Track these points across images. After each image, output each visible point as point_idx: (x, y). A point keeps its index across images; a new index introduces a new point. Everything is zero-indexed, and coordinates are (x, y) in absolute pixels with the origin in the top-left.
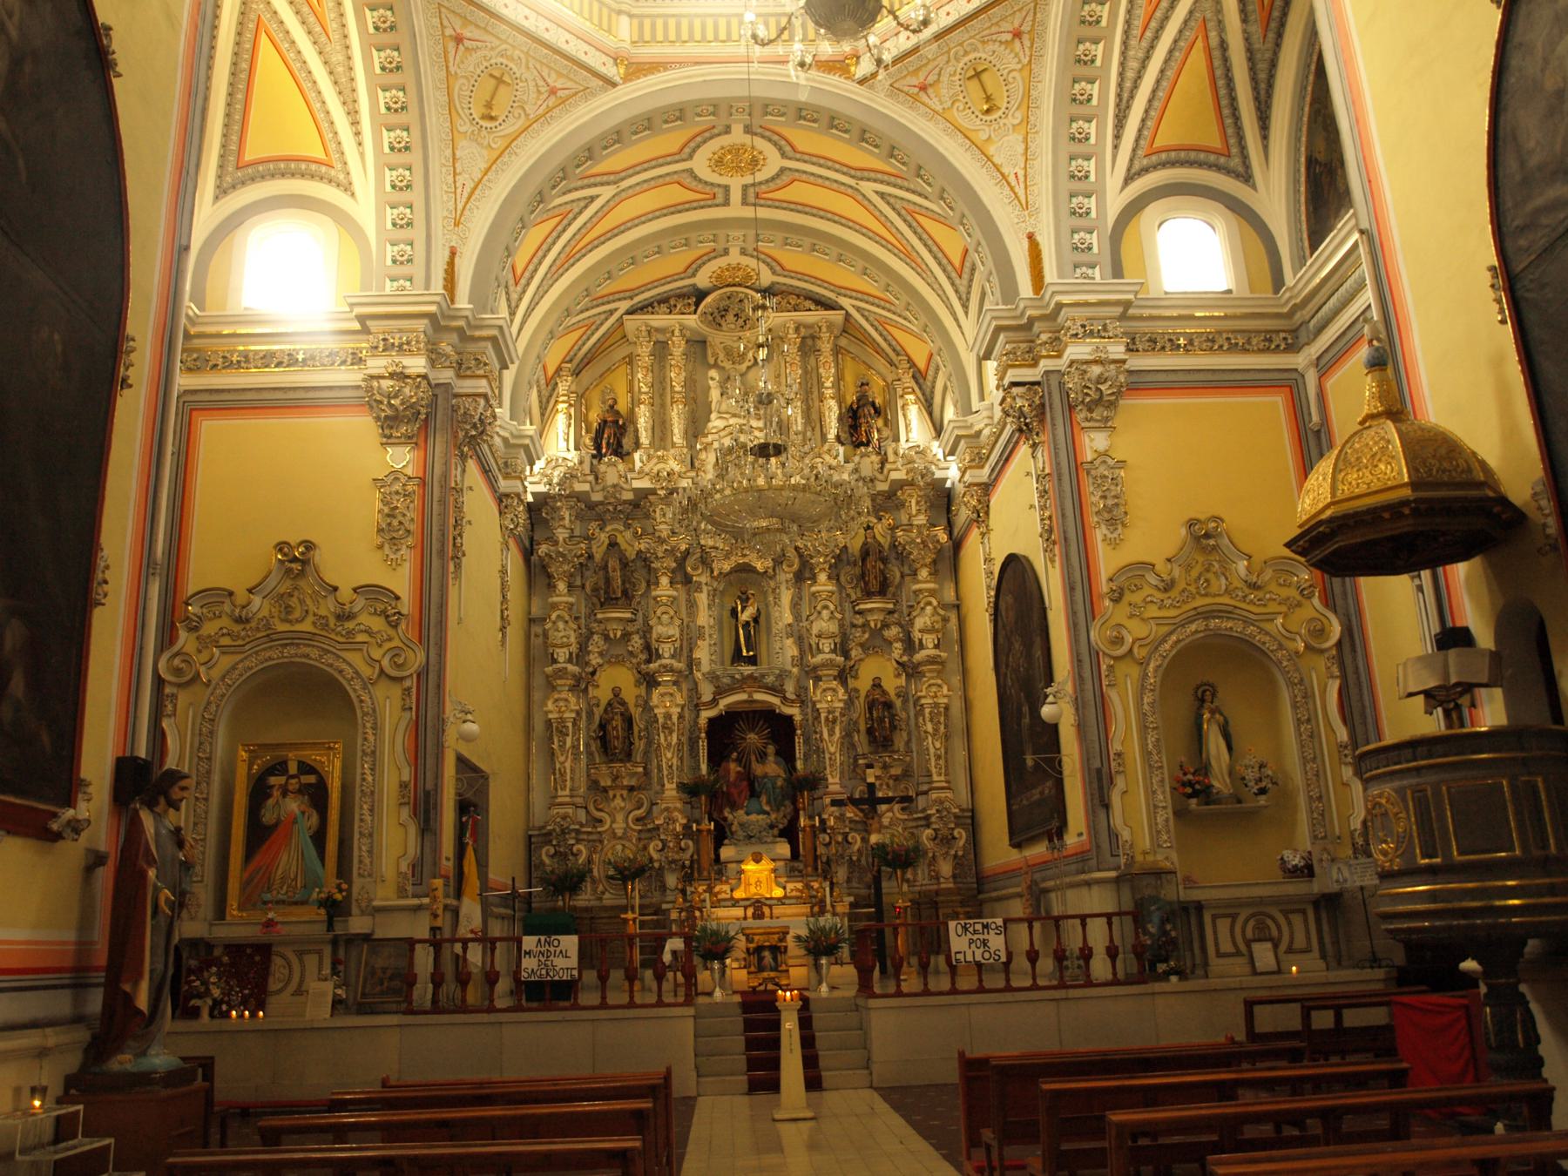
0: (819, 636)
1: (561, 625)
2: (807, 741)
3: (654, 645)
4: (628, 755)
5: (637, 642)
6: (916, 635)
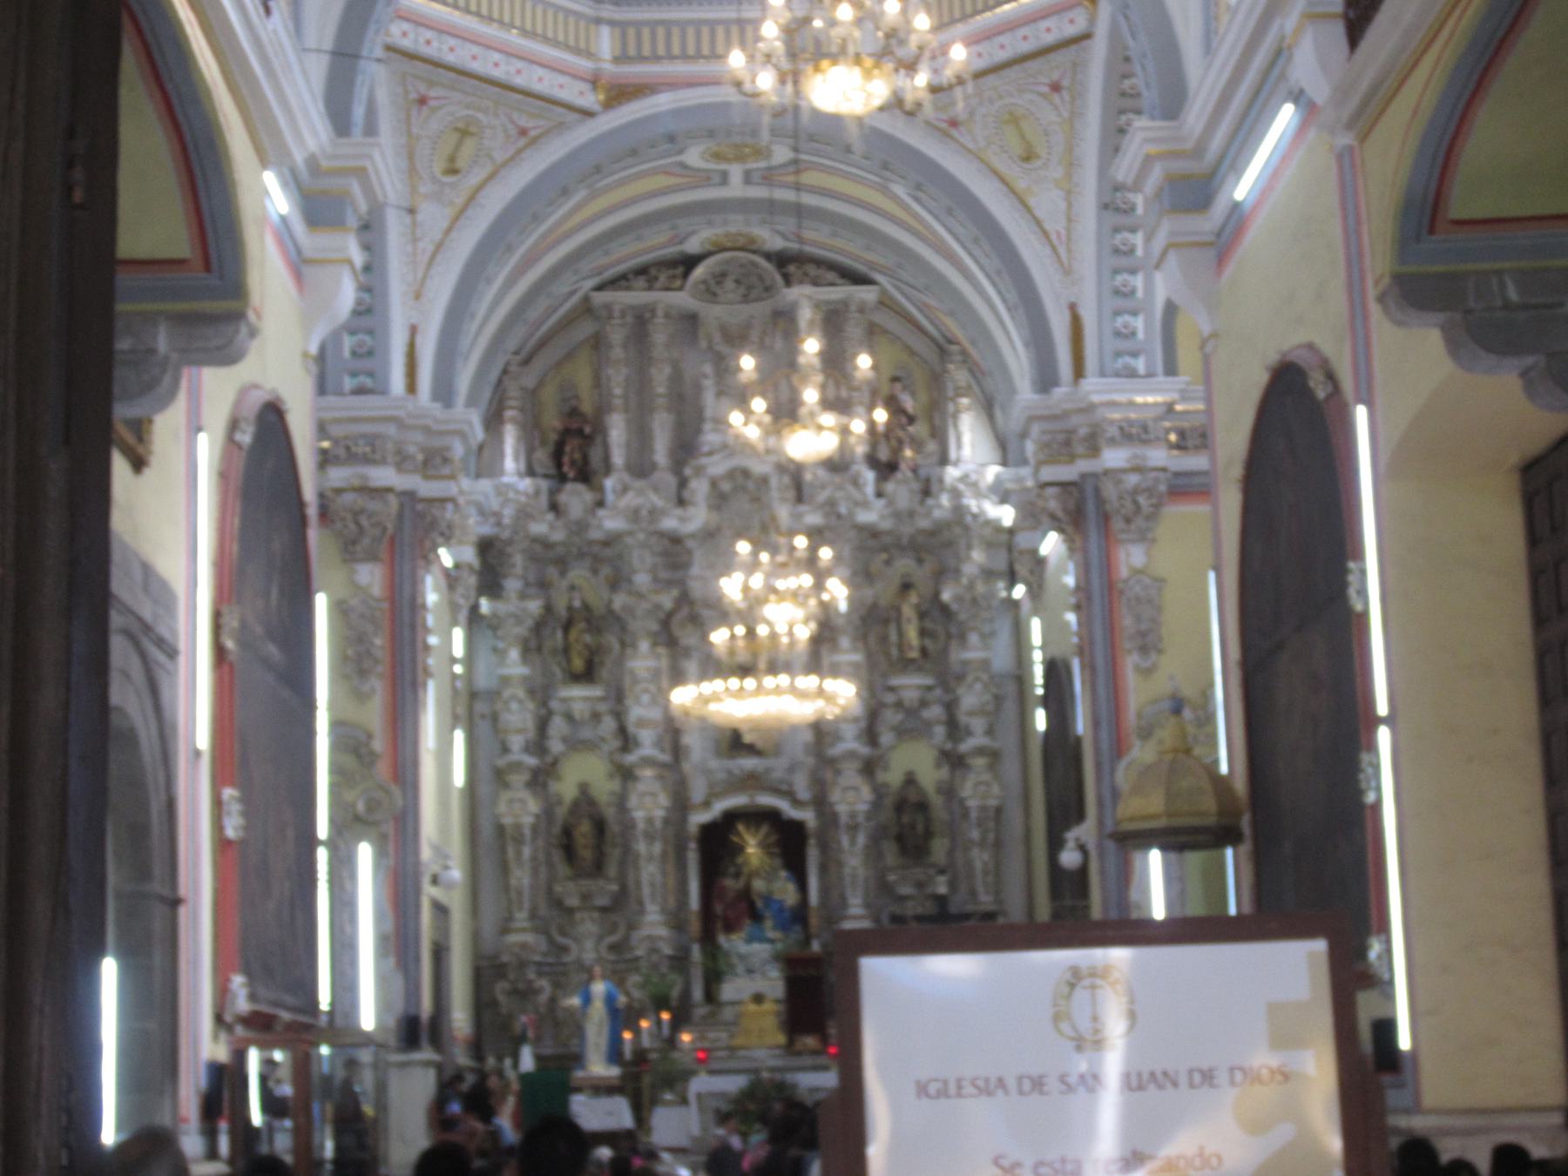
3: (631, 729)
4: (598, 868)
5: (609, 724)
6: (963, 719)
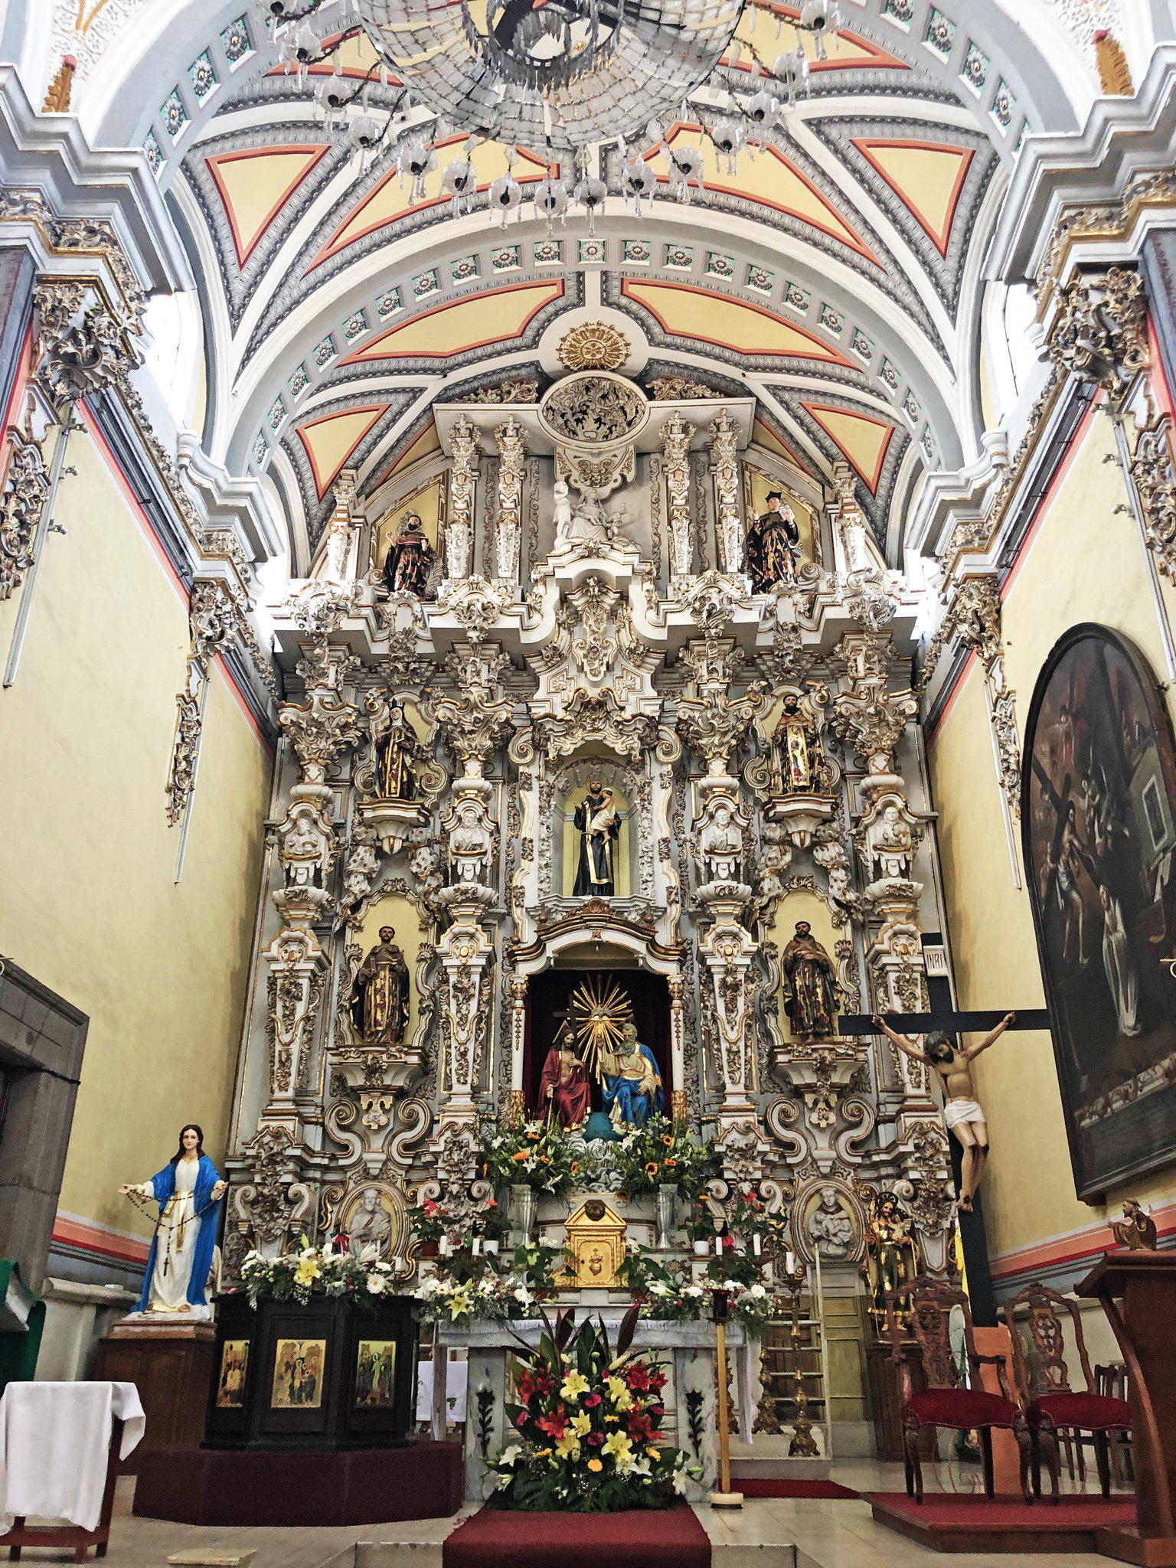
0: (711, 852)
1: (304, 824)
2: (691, 1024)
6: (870, 855)
